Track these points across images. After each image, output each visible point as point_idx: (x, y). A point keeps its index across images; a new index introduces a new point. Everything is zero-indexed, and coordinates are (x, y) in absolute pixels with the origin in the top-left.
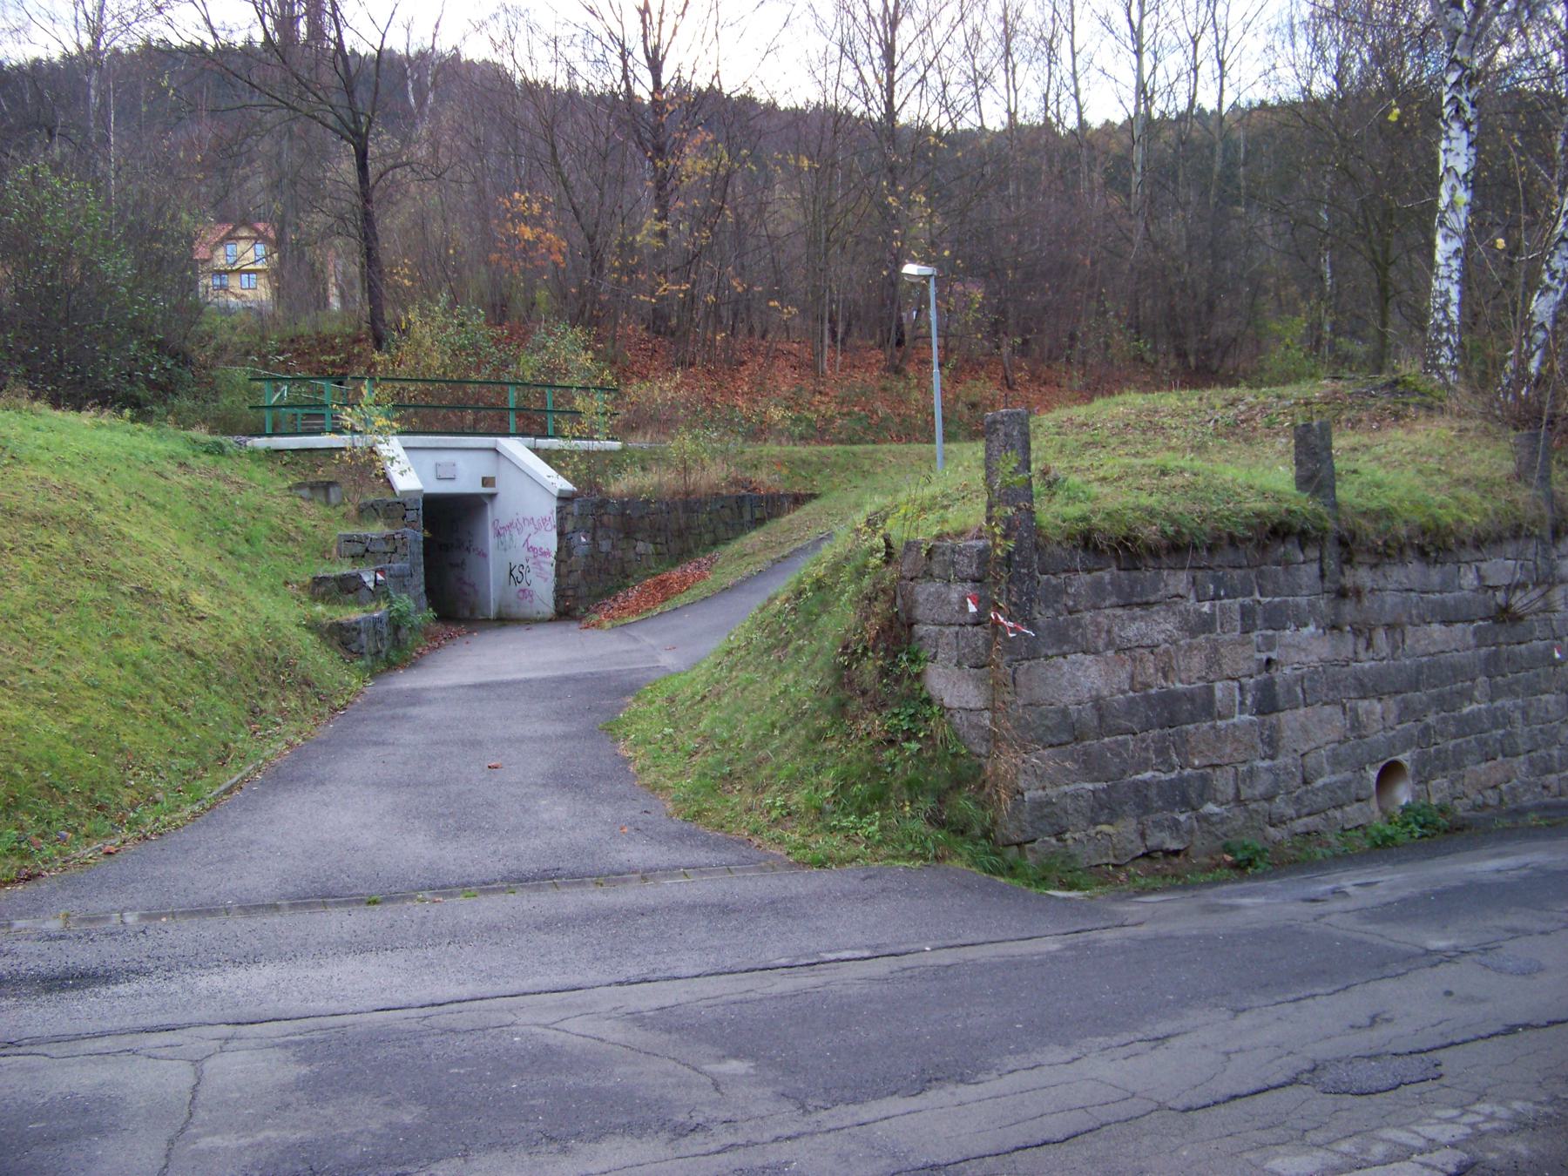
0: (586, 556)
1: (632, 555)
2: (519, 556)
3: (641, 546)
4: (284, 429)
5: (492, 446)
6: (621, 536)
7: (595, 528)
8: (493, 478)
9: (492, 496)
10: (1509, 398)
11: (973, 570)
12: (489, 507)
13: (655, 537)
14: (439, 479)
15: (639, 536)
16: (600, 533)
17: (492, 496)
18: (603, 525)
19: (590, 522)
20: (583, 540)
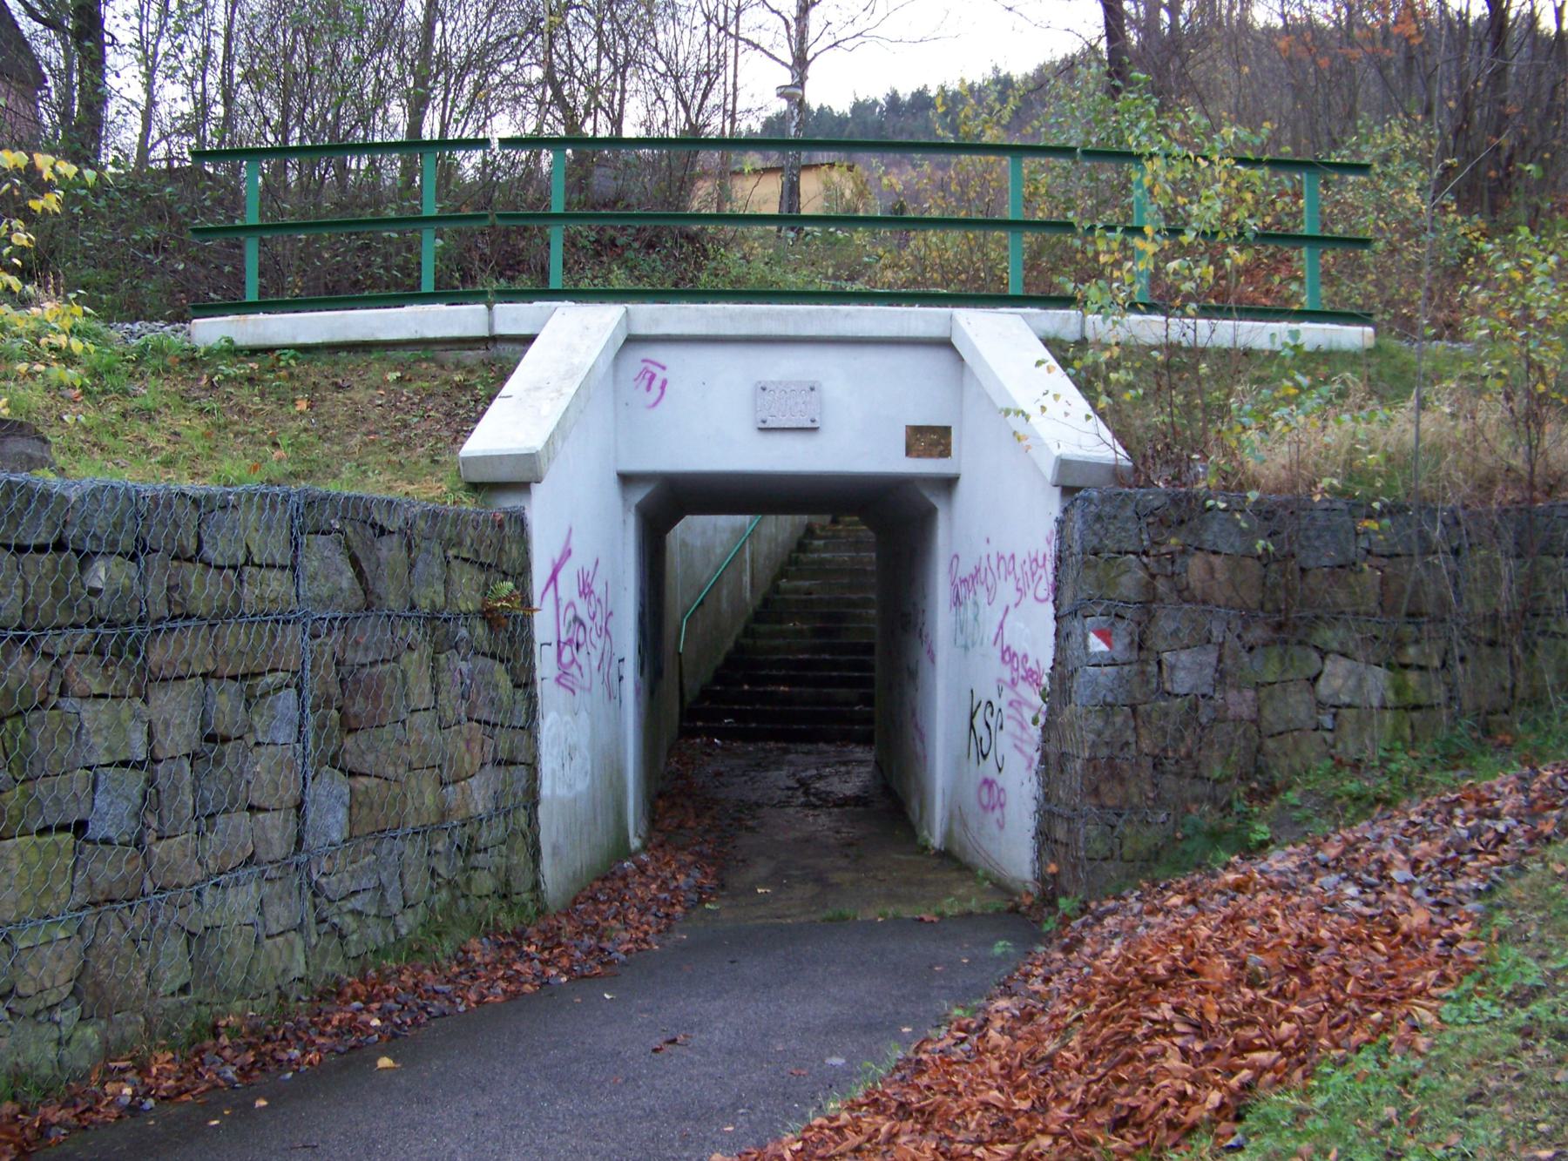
0: (1107, 708)
1: (1297, 706)
2: (988, 674)
3: (1337, 678)
4: (294, 284)
5: (936, 331)
6: (1257, 633)
7: (1148, 604)
8: (946, 431)
9: (948, 484)
10: (1296, 1009)
11: (1010, 92)
12: (941, 517)
13: (1400, 644)
14: (765, 430)
15: (1327, 636)
16: (1165, 623)
17: (948, 484)
18: (1183, 593)
19: (1129, 582)
20: (1097, 645)
